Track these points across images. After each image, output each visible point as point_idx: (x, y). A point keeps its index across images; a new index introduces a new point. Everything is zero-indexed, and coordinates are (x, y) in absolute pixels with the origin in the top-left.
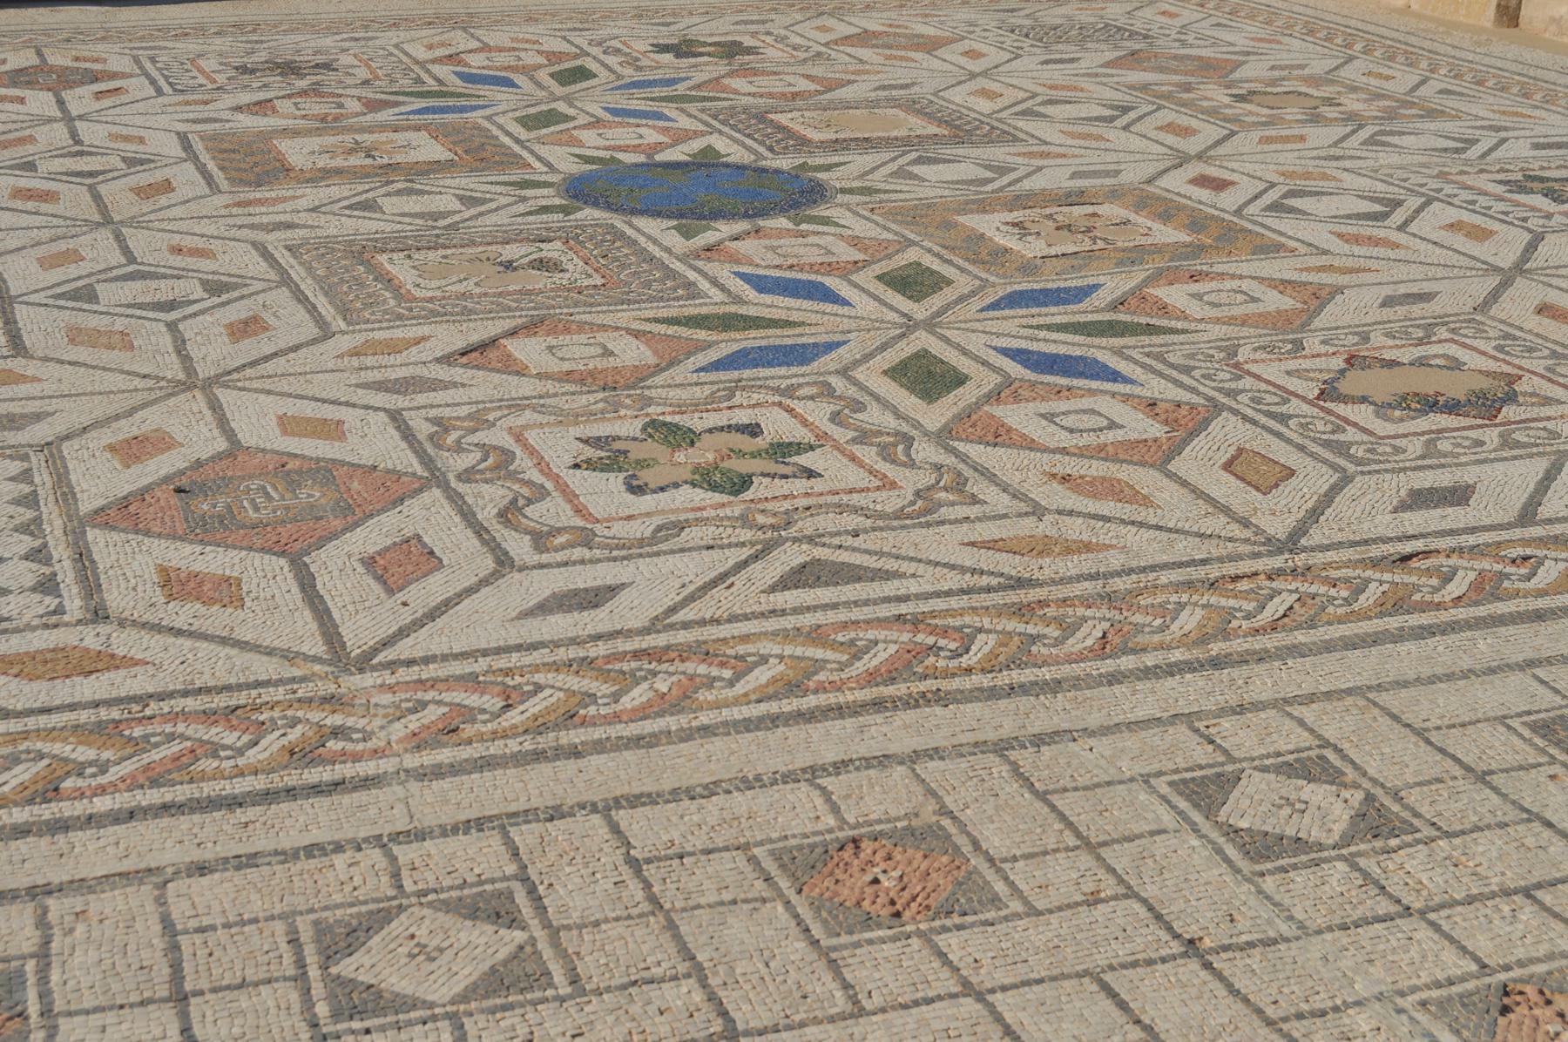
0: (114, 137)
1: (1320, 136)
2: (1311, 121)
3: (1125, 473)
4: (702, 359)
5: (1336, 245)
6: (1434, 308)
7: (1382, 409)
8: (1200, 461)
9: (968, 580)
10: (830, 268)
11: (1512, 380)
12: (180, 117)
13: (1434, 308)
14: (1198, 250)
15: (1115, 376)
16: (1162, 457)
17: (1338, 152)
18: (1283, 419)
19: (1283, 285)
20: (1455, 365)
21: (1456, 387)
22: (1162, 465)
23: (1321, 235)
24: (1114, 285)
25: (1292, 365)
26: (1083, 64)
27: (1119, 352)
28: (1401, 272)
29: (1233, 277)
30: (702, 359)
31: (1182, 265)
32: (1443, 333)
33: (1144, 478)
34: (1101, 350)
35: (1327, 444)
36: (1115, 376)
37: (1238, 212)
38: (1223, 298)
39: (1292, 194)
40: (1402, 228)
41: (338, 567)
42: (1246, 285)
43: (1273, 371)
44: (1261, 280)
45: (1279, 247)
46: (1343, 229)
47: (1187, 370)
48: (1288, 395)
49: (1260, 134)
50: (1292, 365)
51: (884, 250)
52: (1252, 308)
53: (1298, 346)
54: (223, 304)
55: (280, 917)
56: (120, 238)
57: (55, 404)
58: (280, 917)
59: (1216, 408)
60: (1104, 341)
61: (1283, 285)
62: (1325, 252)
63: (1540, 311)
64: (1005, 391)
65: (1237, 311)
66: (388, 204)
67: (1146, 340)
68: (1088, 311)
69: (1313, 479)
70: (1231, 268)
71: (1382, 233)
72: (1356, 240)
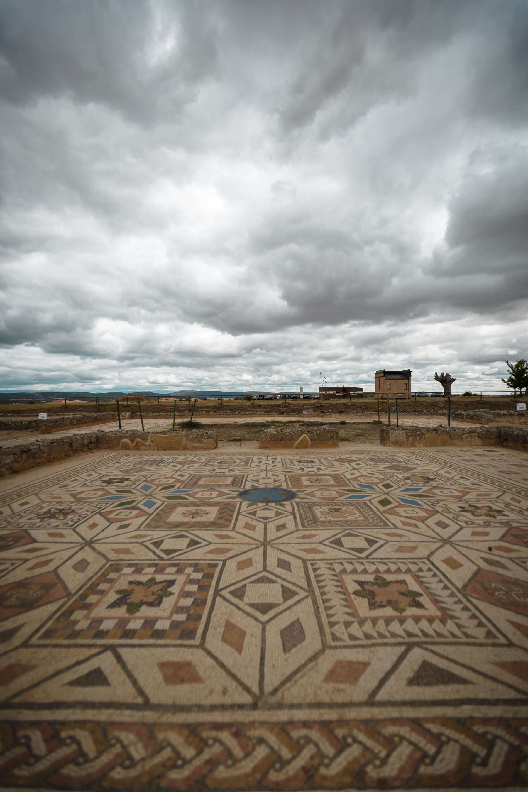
0: (273, 475)
4: (347, 496)
8: (431, 522)
10: (372, 484)
12: (230, 541)
16: (423, 520)
22: (423, 522)
30: (347, 496)
33: (419, 524)
34: (418, 500)
41: (271, 527)
51: (383, 480)
52: (452, 494)
54: (197, 560)
55: (138, 762)
57: (297, 541)
58: (138, 762)
60: (419, 498)
64: (400, 506)
65: (448, 495)
66: (315, 469)
67: (427, 498)
69: (454, 527)
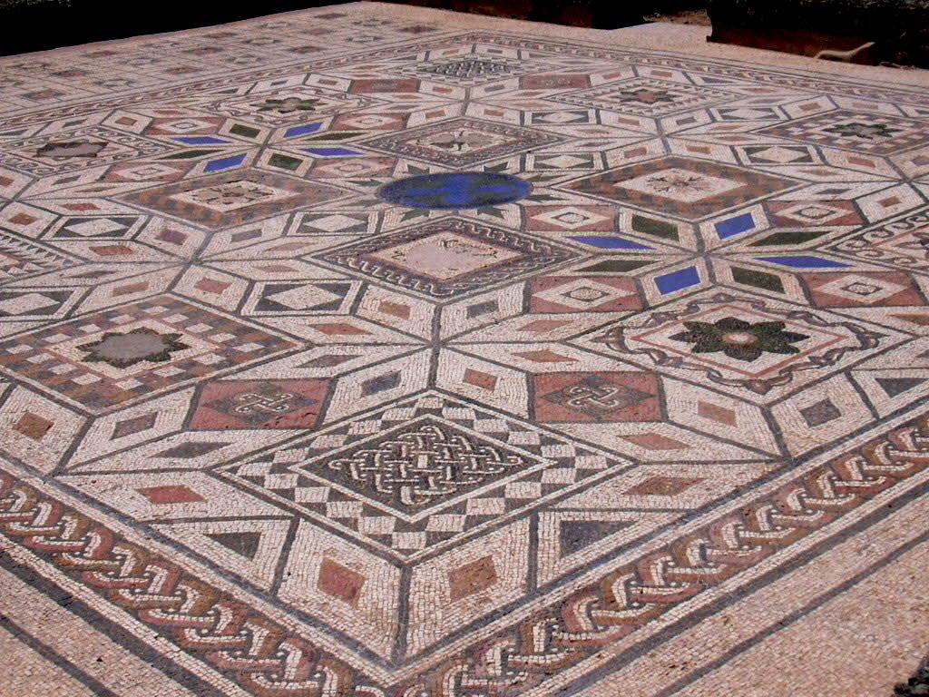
1: (102, 298)
2: (109, 315)
3: (165, 116)
5: (96, 202)
6: (57, 178)
7: (87, 142)
9: (39, 324)
11: (38, 156)
13: (57, 178)
14: (168, 191)
15: (181, 140)
17: (90, 282)
18: (119, 134)
19: (122, 180)
20: (56, 158)
21: (60, 151)
22: (154, 119)
23: (105, 207)
24: (198, 171)
25: (116, 152)
26: (81, 181)
27: (182, 147)
28: (254, 251)
29: (145, 180)
31: (173, 184)
32: (55, 169)
35: (105, 130)
36: (181, 140)
37: (151, 216)
38: (148, 172)
39: (121, 233)
40: (61, 216)
42: (139, 178)
43: (123, 149)
44: (133, 181)
45: (127, 199)
46: (92, 212)
47: (156, 145)
48: (120, 142)
49: (147, 293)
50: (116, 152)
53: (115, 158)
56: (665, 143)
59: (142, 134)
61: (122, 180)
62: (103, 198)
63: (233, 240)
65: (142, 167)
68: (203, 161)
70: (147, 184)
71: (71, 213)
72: (85, 207)
